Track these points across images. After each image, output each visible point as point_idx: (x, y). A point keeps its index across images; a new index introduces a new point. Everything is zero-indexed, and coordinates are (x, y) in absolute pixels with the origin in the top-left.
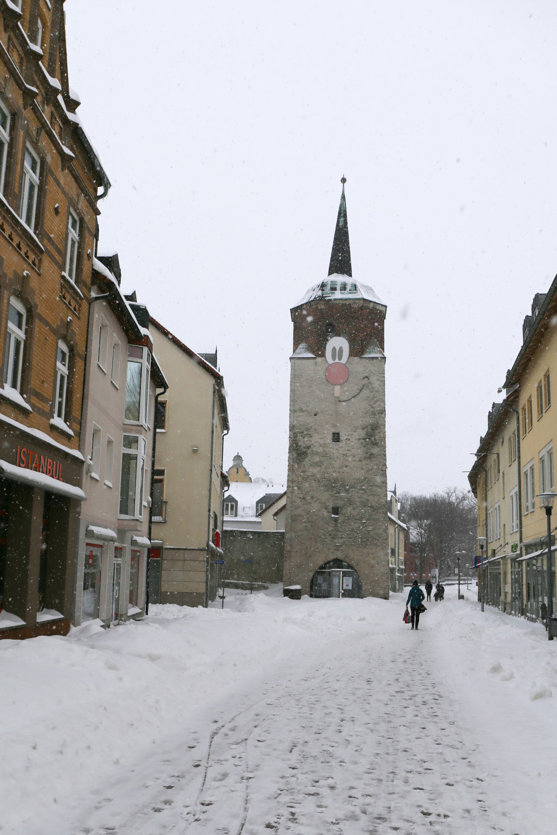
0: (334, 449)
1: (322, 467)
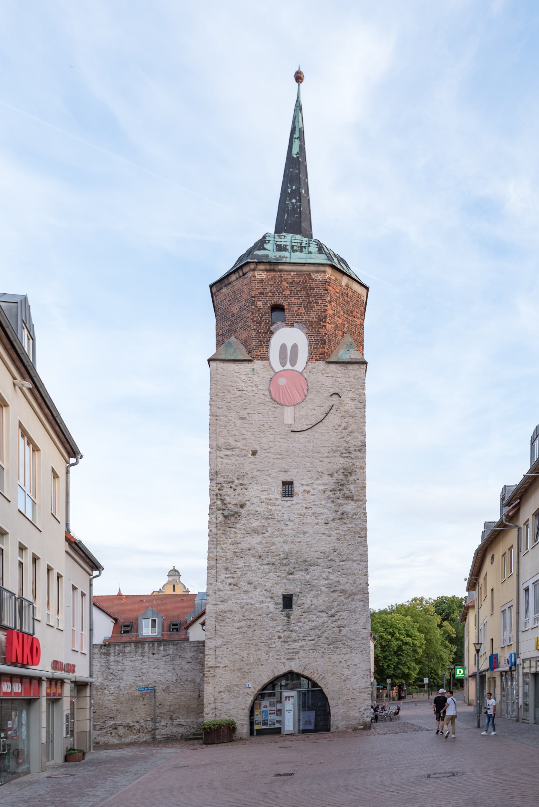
0: (285, 508)
1: (265, 535)
